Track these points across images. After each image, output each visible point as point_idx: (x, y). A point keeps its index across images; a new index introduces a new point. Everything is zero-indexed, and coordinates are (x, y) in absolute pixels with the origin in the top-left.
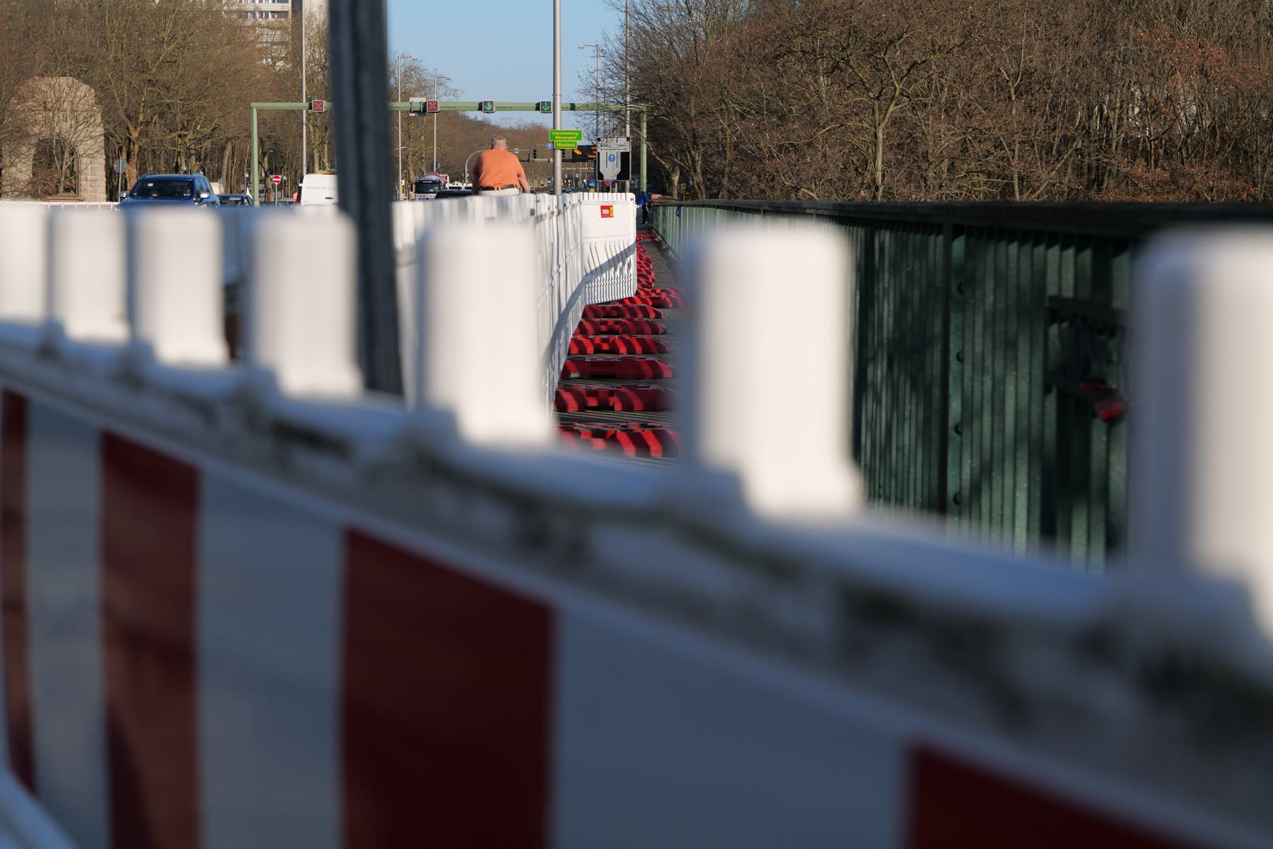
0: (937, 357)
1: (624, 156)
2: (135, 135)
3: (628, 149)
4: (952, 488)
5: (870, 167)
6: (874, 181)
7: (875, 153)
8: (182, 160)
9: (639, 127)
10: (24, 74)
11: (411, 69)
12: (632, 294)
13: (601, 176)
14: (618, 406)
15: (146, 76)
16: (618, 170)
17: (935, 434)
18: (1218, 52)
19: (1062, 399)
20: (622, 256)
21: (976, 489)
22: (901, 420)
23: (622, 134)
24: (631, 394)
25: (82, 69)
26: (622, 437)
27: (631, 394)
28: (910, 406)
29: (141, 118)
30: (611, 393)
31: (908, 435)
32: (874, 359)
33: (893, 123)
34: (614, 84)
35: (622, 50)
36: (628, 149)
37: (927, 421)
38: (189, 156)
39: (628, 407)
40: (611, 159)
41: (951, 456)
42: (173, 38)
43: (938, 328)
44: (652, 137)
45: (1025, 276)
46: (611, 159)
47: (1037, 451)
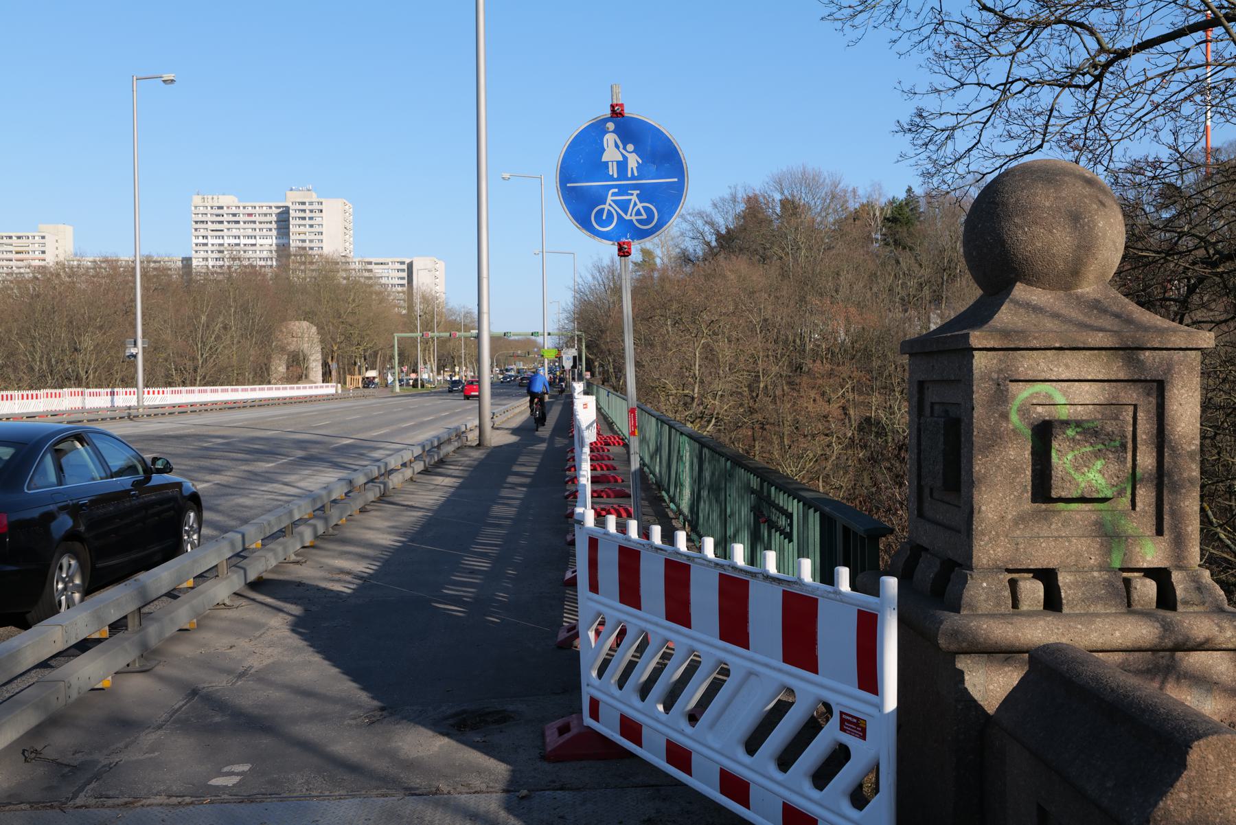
0: (723, 494)
1: (575, 358)
2: (335, 348)
3: (576, 354)
4: (728, 534)
5: (693, 368)
6: (695, 375)
7: (695, 362)
8: (358, 360)
9: (582, 345)
10: (284, 319)
11: (467, 313)
12: (595, 440)
13: (563, 367)
14: (605, 496)
15: (340, 320)
16: (572, 364)
17: (723, 517)
18: (853, 310)
19: (754, 514)
20: (591, 425)
21: (735, 536)
22: (713, 512)
23: (574, 347)
24: (609, 492)
25: (309, 316)
26: (612, 510)
27: (609, 492)
28: (716, 507)
29: (338, 340)
30: (602, 491)
31: (715, 516)
32: (703, 488)
33: (703, 348)
34: (570, 326)
35: (573, 308)
36: (576, 354)
37: (721, 515)
38: (360, 358)
39: (608, 496)
40: (568, 359)
41: (728, 525)
42: (354, 300)
43: (723, 485)
44: (587, 347)
45: (746, 479)
46: (568, 359)
47: (749, 526)
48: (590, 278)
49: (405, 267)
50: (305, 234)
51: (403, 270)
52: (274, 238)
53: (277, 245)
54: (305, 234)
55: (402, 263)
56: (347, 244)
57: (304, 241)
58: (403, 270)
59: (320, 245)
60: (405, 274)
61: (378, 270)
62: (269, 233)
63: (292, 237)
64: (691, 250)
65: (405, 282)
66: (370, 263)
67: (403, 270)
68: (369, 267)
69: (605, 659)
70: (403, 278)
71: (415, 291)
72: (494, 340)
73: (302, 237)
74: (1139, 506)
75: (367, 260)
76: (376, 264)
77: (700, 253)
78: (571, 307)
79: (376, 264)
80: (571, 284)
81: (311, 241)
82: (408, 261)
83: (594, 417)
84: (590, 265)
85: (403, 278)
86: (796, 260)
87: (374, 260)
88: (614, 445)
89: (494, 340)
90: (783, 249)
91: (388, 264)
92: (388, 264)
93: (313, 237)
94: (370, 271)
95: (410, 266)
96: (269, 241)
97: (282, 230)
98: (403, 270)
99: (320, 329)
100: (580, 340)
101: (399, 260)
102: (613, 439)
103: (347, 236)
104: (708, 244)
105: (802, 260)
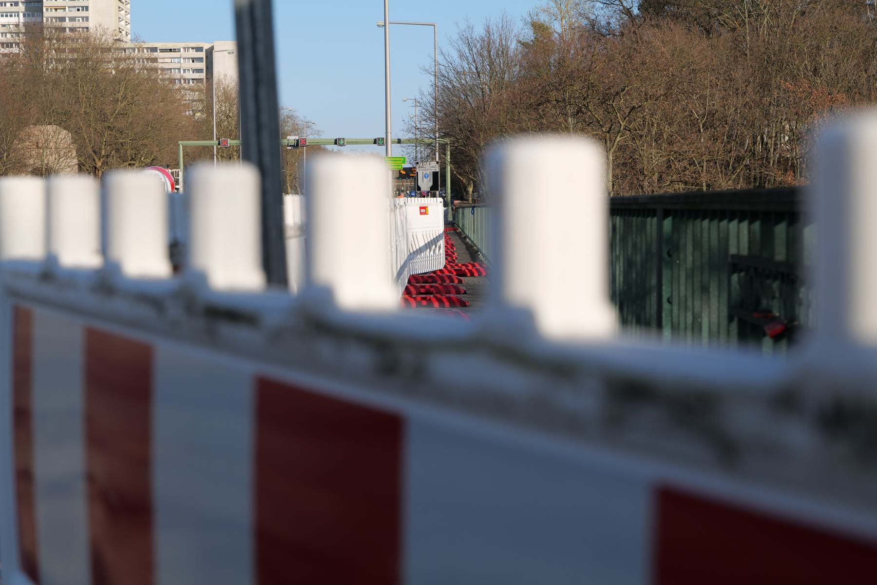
1: (435, 174)
3: (438, 170)
10: (23, 124)
16: (431, 184)
23: (433, 159)
25: (63, 120)
29: (103, 153)
34: (427, 125)
36: (438, 170)
40: (425, 176)
46: (425, 176)
48: (455, 55)
49: (202, 55)
50: (64, 9)
51: (200, 59)
52: (21, 15)
53: (26, 25)
54: (64, 9)
55: (199, 49)
56: (123, 23)
57: (62, 19)
58: (200, 60)
59: (85, 25)
60: (202, 65)
61: (165, 61)
62: (14, 9)
63: (46, 14)
64: (603, 23)
65: (203, 75)
66: (154, 50)
67: (200, 60)
68: (155, 54)
69: (444, 210)
70: (199, 71)
71: (215, 86)
72: (203, 62)
73: (60, 13)
74: (412, 233)
75: (151, 45)
76: (162, 51)
77: (615, 24)
78: (428, 99)
79: (162, 51)
80: (429, 63)
81: (72, 19)
82: (206, 46)
83: (440, 228)
84: (456, 37)
85: (199, 71)
86: (755, 30)
87: (159, 45)
88: (472, 275)
89: (203, 62)
90: (737, 16)
91: (179, 51)
92: (179, 51)
93: (74, 14)
94: (155, 60)
95: (210, 53)
96: (13, 20)
97: (32, 5)
98: (200, 59)
99: (77, 133)
100: (443, 148)
101: (194, 45)
102: (470, 267)
103: (123, 12)
104: (628, 12)
105: (763, 31)
